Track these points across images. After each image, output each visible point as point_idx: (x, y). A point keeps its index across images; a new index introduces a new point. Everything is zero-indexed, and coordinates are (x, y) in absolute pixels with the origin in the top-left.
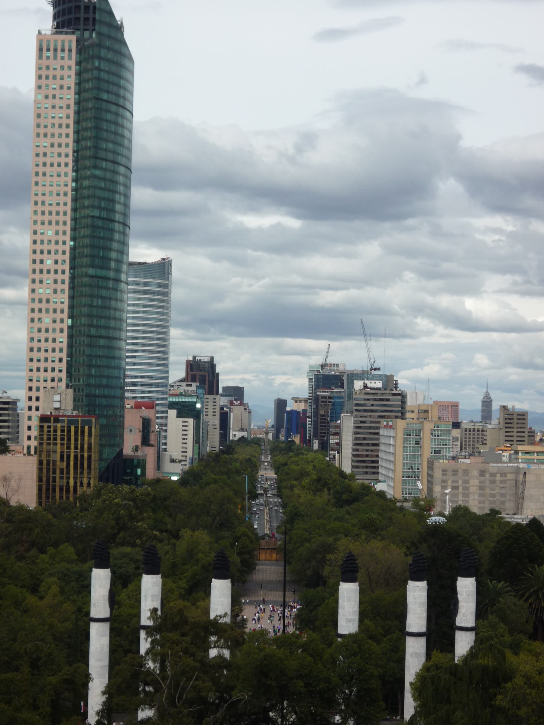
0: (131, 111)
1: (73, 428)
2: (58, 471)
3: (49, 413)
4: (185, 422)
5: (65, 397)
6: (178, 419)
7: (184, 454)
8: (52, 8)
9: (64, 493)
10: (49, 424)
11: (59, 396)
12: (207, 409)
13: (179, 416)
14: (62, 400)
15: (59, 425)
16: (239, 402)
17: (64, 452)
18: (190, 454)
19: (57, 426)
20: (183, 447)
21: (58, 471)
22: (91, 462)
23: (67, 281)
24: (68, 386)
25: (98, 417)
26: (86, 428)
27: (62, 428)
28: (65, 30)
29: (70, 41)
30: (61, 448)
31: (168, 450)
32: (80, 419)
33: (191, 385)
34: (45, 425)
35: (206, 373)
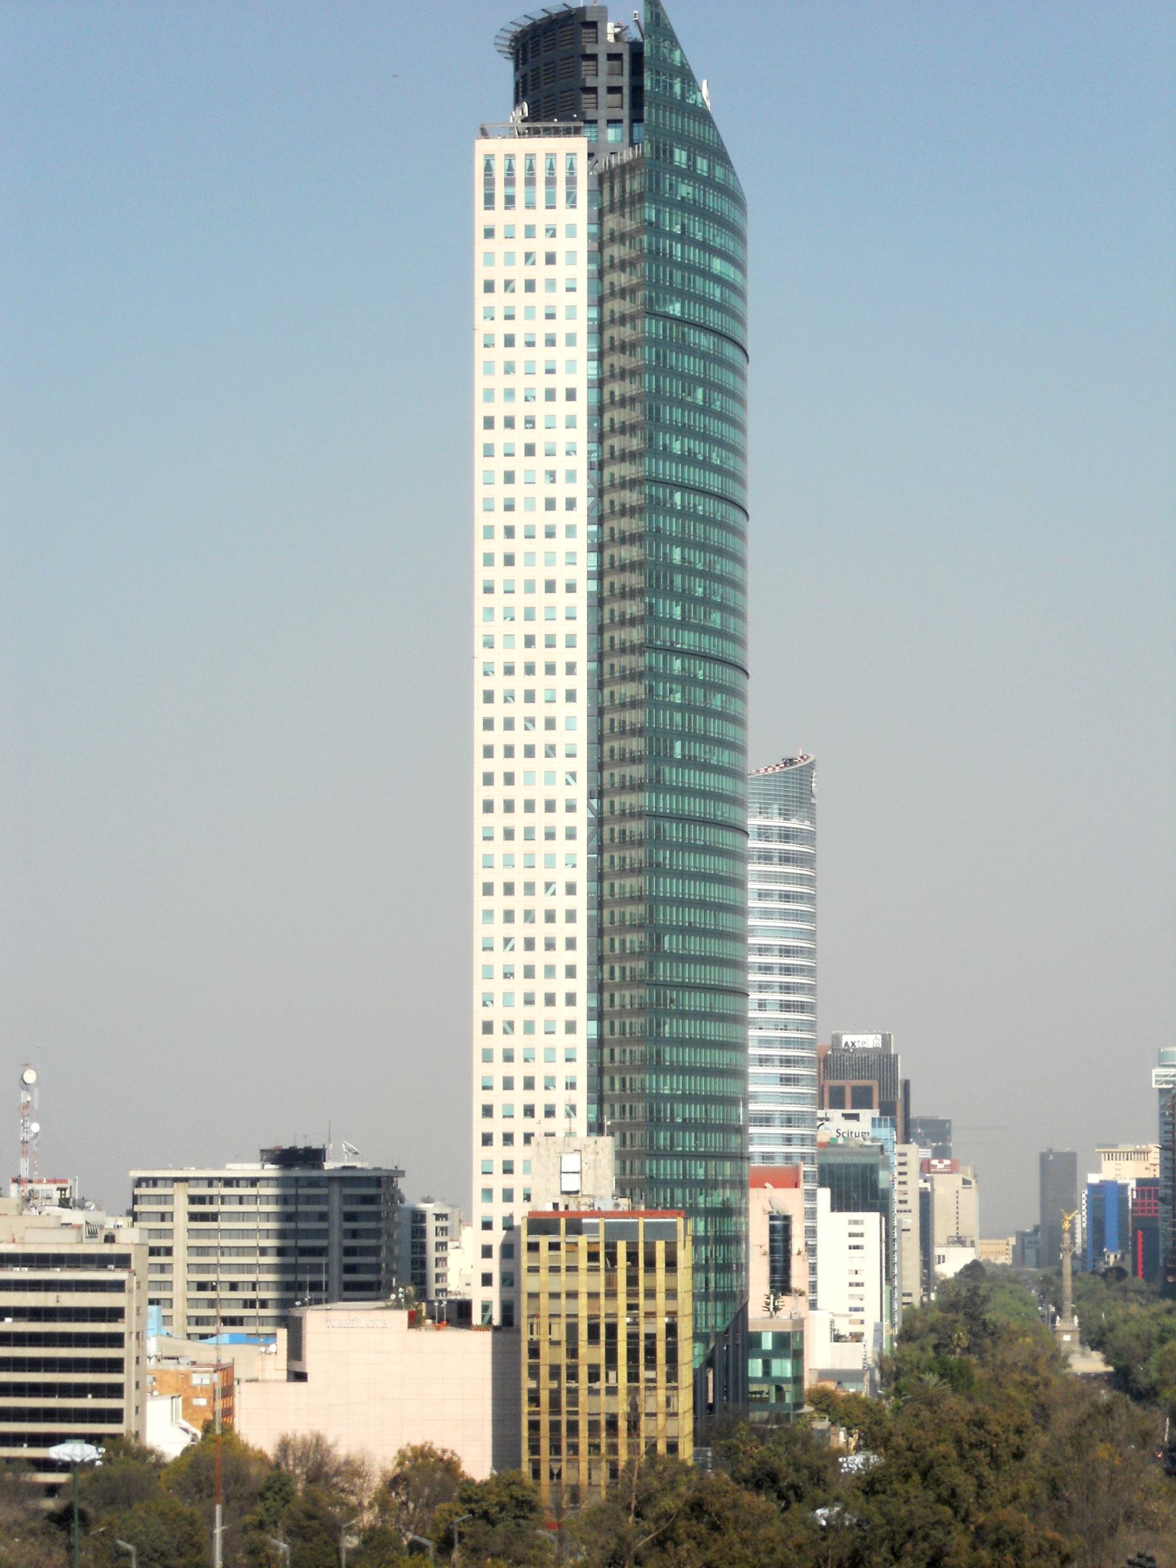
0: (741, 342)
1: (622, 1249)
2: (583, 1373)
3: (549, 1208)
4: (856, 1222)
5: (595, 1161)
6: (837, 1214)
7: (857, 1316)
8: (510, 66)
9: (603, 1434)
10: (553, 1239)
11: (577, 1156)
12: (904, 1183)
13: (838, 1204)
14: (585, 1167)
15: (583, 1240)
16: (947, 1162)
17: (598, 1317)
18: (872, 1314)
19: (576, 1244)
20: (851, 1296)
21: (583, 1373)
22: (615, 1344)
23: (583, 832)
24: (596, 1128)
25: (691, 1212)
26: (660, 1246)
27: (593, 1249)
28: (555, 123)
29: (571, 155)
30: (590, 1308)
31: (819, 1305)
32: (641, 1221)
33: (856, 1117)
34: (544, 1241)
35: (874, 1083)
